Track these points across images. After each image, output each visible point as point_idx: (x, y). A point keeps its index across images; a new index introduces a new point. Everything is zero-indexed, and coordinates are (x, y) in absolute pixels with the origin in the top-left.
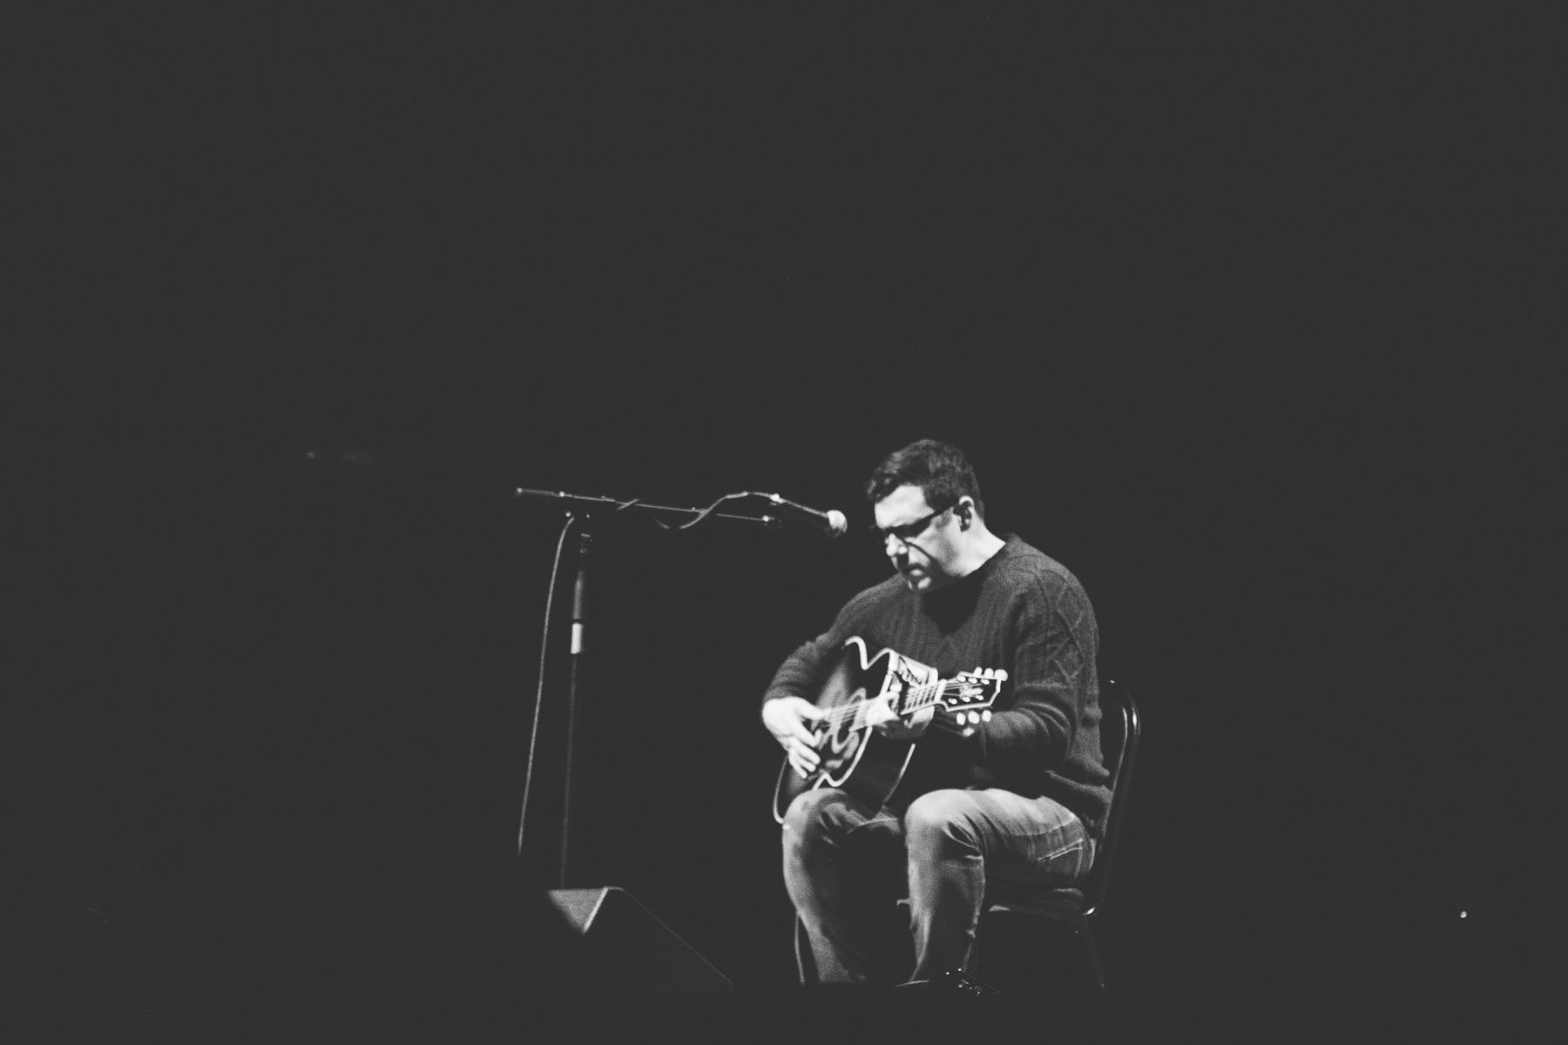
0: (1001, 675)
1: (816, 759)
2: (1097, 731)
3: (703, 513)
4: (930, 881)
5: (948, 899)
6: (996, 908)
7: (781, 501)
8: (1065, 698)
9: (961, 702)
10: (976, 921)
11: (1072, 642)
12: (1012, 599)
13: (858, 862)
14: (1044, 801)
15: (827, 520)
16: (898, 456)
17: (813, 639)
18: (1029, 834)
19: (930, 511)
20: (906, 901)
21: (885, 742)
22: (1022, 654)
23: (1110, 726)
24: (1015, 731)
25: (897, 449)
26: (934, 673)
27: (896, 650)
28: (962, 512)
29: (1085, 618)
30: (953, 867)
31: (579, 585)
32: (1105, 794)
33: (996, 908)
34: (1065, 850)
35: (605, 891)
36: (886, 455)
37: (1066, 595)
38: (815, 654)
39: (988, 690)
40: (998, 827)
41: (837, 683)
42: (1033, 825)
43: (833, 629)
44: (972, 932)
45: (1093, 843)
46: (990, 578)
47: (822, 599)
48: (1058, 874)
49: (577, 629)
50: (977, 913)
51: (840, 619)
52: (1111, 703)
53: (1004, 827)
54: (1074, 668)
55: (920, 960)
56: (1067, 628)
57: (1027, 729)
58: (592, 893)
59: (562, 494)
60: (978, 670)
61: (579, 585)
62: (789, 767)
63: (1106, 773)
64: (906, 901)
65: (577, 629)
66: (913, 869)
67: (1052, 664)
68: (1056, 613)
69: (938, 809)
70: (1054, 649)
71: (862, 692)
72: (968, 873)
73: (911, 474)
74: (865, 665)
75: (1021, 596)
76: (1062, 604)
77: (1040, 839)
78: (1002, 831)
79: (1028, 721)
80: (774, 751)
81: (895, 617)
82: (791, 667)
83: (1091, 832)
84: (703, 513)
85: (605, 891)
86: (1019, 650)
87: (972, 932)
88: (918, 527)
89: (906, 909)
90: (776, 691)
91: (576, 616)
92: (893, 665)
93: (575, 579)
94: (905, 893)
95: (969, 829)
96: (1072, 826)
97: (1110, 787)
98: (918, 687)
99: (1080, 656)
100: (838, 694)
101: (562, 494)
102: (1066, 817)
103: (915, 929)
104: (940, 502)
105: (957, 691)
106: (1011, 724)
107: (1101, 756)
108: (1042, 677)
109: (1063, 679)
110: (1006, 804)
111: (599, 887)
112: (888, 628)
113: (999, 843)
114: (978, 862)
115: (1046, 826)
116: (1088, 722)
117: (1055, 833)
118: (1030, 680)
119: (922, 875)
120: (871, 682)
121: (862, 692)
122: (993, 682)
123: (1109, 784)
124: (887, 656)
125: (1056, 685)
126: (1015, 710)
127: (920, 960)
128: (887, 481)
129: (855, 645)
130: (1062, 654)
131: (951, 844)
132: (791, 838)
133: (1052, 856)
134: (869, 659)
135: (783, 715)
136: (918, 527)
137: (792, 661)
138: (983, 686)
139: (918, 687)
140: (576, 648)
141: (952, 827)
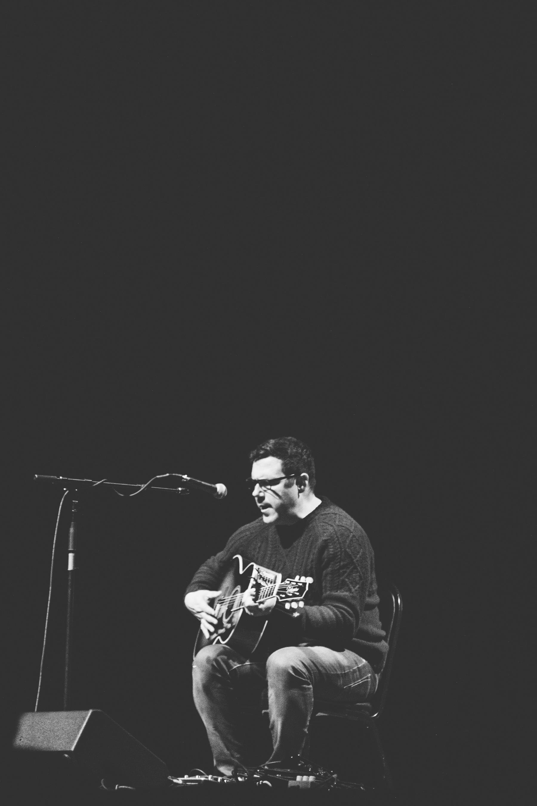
0: (309, 580)
1: (212, 629)
2: (377, 610)
3: (143, 486)
4: (282, 699)
5: (291, 711)
6: (319, 714)
7: (189, 478)
8: (354, 602)
9: (287, 597)
10: (308, 723)
11: (355, 568)
12: (320, 541)
13: (239, 688)
14: (347, 652)
15: (216, 489)
16: (272, 441)
17: (215, 555)
18: (339, 673)
19: (283, 476)
20: (268, 711)
21: (252, 619)
22: (327, 575)
23: (385, 607)
24: (324, 618)
25: (273, 438)
26: (280, 576)
27: (256, 563)
28: (301, 483)
29: (364, 553)
30: (295, 692)
31: (72, 530)
32: (384, 646)
33: (319, 714)
34: (360, 681)
35: (90, 712)
36: (265, 440)
37: (351, 540)
38: (216, 564)
39: (302, 589)
40: (320, 668)
41: (228, 582)
42: (341, 667)
43: (226, 549)
44: (306, 730)
45: (377, 677)
46: (310, 526)
47: (219, 533)
48: (357, 694)
49: (71, 556)
50: (309, 718)
51: (229, 544)
52: (385, 594)
53: (322, 667)
54: (357, 584)
55: (275, 747)
56: (352, 560)
57: (330, 618)
58: (83, 713)
59: (61, 478)
60: (297, 577)
61: (72, 530)
62: (201, 631)
63: (383, 633)
64: (268, 711)
65: (71, 556)
66: (271, 693)
67: (343, 581)
68: (345, 551)
69: (284, 658)
70: (345, 572)
71: (238, 588)
72: (304, 696)
73: (275, 453)
74: (241, 572)
75: (326, 540)
76: (349, 547)
77: (346, 675)
78: (324, 671)
79: (331, 613)
80: (193, 621)
81: (259, 545)
82: (202, 572)
83: (375, 670)
84: (143, 486)
85: (90, 712)
86: (324, 572)
87: (306, 730)
88: (275, 482)
89: (267, 715)
90: (193, 586)
91: (71, 549)
92: (255, 574)
93: (70, 527)
94: (267, 706)
95: (304, 670)
96: (364, 666)
97: (386, 641)
98: (270, 586)
99: (360, 576)
100: (228, 588)
101: (61, 478)
102: (361, 662)
103: (273, 727)
104: (290, 471)
105: (285, 589)
106: (322, 614)
107: (380, 623)
108: (337, 589)
109: (350, 590)
110: (324, 654)
111: (88, 709)
112: (255, 549)
113: (318, 674)
114: (309, 689)
115: (349, 667)
116: (370, 607)
117: (354, 671)
118: (331, 590)
119: (277, 696)
120: (242, 582)
121: (238, 588)
122: (305, 584)
123: (385, 638)
124: (252, 566)
125: (347, 593)
126: (324, 605)
127: (275, 747)
128: (262, 452)
129: (237, 558)
130: (349, 575)
131: (292, 679)
132: (198, 676)
133: (352, 685)
134: (243, 569)
135: (196, 600)
136: (275, 482)
137: (204, 568)
138: (299, 587)
139: (270, 586)
140: (70, 567)
141: (294, 668)
